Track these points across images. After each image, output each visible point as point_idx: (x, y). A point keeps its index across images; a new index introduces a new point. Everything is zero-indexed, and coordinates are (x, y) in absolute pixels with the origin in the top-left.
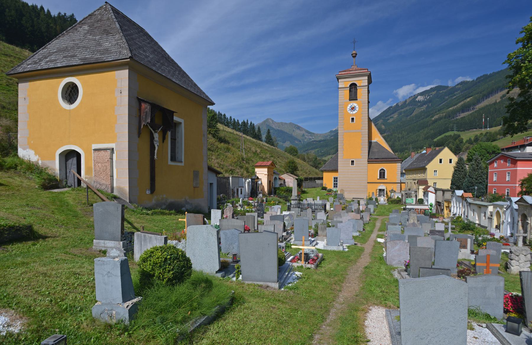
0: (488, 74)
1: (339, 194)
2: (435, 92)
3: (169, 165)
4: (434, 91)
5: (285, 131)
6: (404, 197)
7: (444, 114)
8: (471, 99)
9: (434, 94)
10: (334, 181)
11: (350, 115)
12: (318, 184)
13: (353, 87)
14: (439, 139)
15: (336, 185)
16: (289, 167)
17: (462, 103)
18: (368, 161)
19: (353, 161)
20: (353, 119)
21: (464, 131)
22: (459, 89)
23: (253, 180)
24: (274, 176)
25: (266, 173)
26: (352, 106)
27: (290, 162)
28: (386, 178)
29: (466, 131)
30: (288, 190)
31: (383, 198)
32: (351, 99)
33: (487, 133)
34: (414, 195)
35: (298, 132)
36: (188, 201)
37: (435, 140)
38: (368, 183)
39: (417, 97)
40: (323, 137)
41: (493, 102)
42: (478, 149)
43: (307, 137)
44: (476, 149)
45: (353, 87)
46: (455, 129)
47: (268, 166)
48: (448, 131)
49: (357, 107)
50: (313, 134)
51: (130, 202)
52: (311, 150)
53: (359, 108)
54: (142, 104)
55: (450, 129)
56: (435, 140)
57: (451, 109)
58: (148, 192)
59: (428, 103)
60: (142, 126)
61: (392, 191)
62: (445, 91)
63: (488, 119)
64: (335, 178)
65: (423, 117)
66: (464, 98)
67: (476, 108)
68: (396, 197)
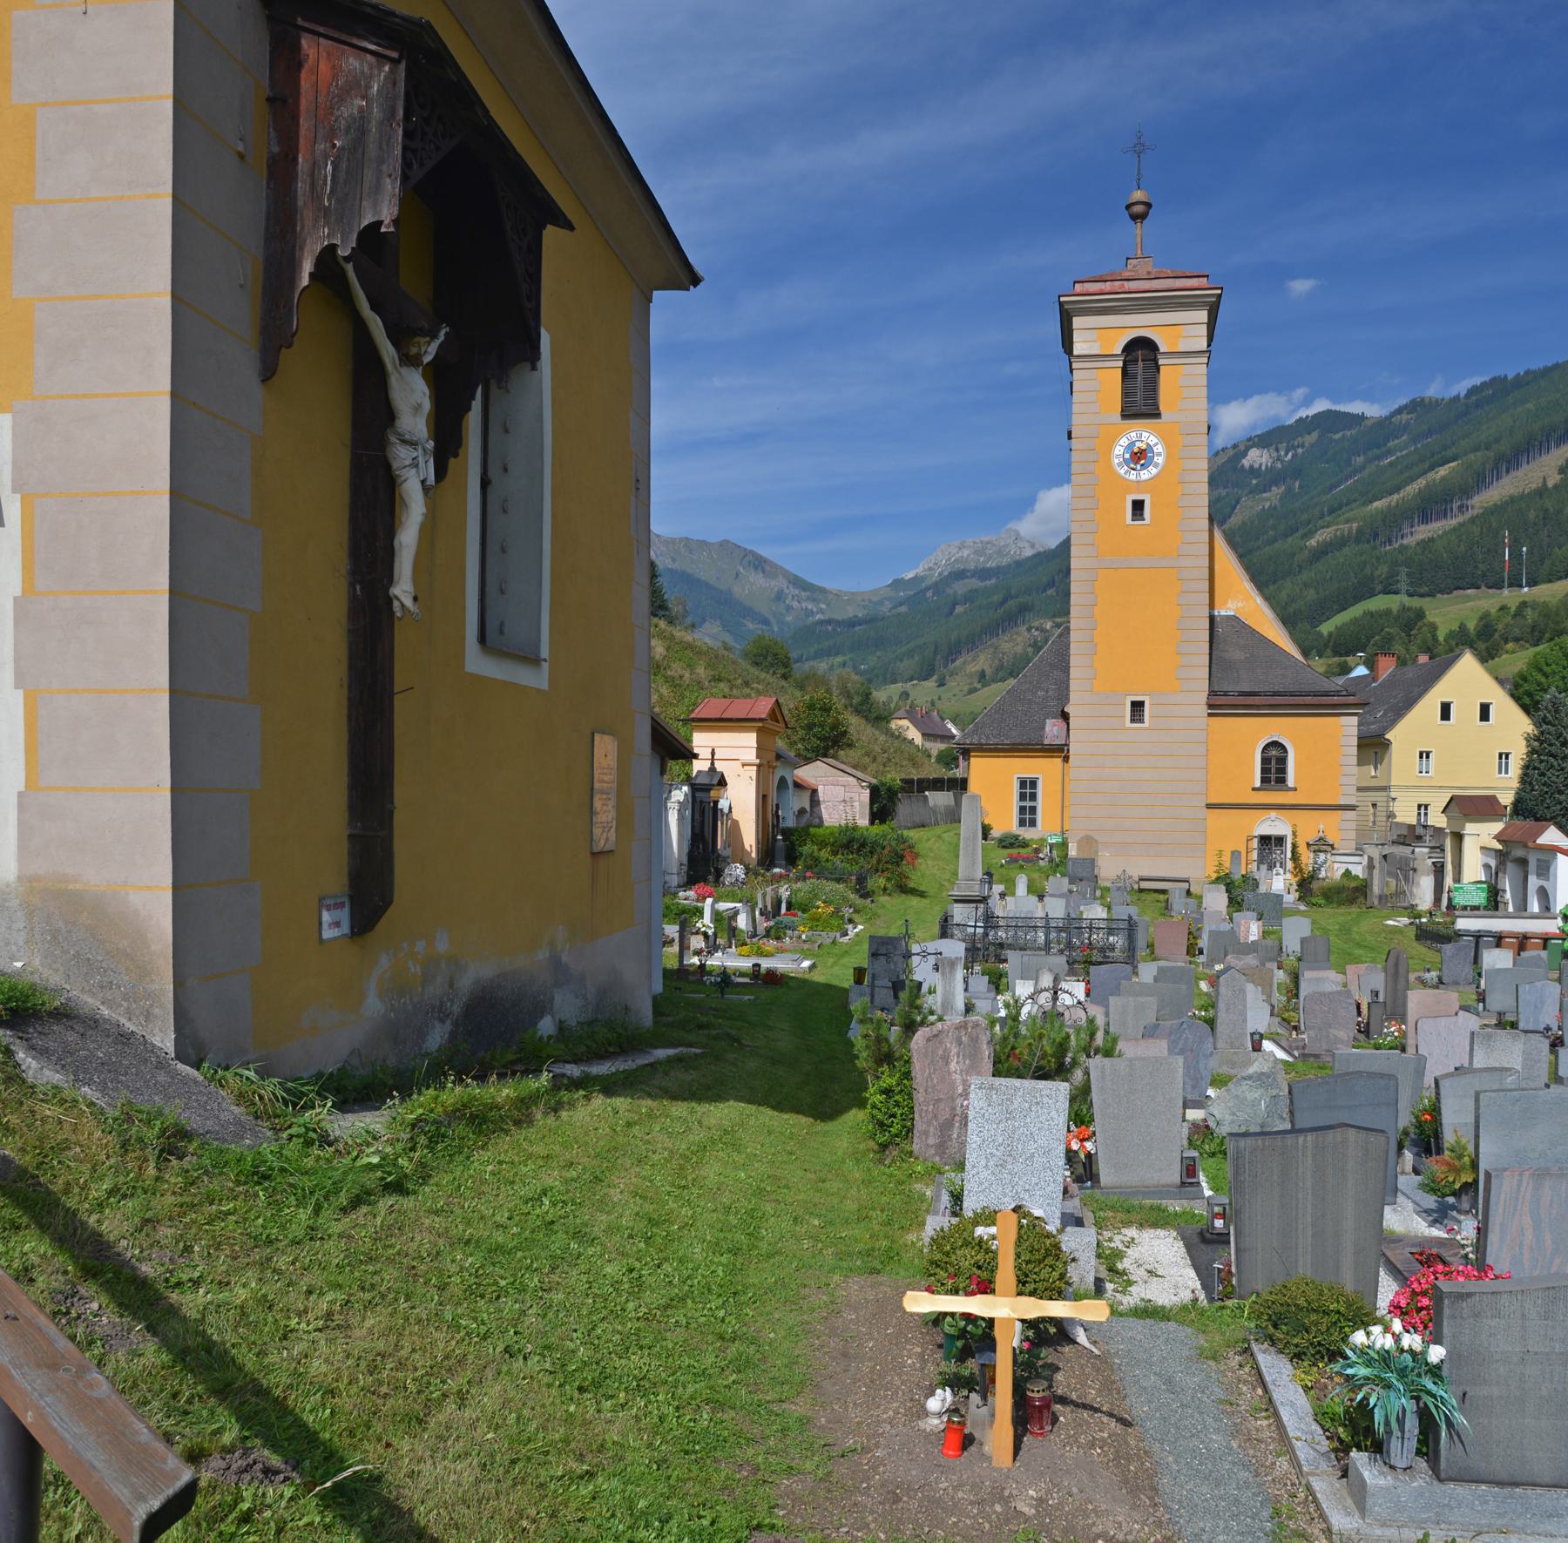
0: (1511, 376)
1: (1075, 860)
2: (1315, 435)
3: (472, 675)
4: (1309, 433)
5: (703, 576)
6: (1376, 872)
7: (1355, 525)
8: (1453, 468)
9: (1312, 445)
10: (1022, 797)
11: (1129, 486)
12: (934, 811)
13: (1141, 353)
14: (1344, 624)
15: (1028, 816)
16: (810, 727)
17: (1421, 483)
18: (1210, 706)
19: (1141, 704)
20: (1138, 506)
21: (1431, 594)
22: (1405, 428)
23: (698, 795)
24: (779, 773)
25: (751, 756)
26: (1133, 443)
27: (811, 707)
28: (1291, 782)
29: (1439, 595)
30: (851, 840)
31: (1281, 878)
32: (1129, 413)
33: (1524, 604)
34: (1429, 862)
35: (757, 580)
36: (564, 959)
37: (1326, 628)
38: (1209, 806)
39: (1245, 454)
40: (864, 607)
41: (1534, 486)
42: (1554, 667)
43: (795, 604)
44: (1548, 665)
45: (1141, 353)
46: (1403, 587)
47: (761, 720)
48: (1372, 594)
49: (1159, 449)
50: (823, 590)
51: (191, 1049)
52: (814, 658)
53: (1169, 457)
54: (306, 42)
55: (1379, 588)
56: (1326, 628)
57: (1377, 504)
58: (333, 924)
59: (1288, 479)
60: (307, 267)
61: (1321, 845)
62: (1353, 432)
63: (1524, 549)
64: (1023, 783)
65: (1271, 533)
66: (1427, 465)
67: (1473, 508)
68: (1338, 874)
